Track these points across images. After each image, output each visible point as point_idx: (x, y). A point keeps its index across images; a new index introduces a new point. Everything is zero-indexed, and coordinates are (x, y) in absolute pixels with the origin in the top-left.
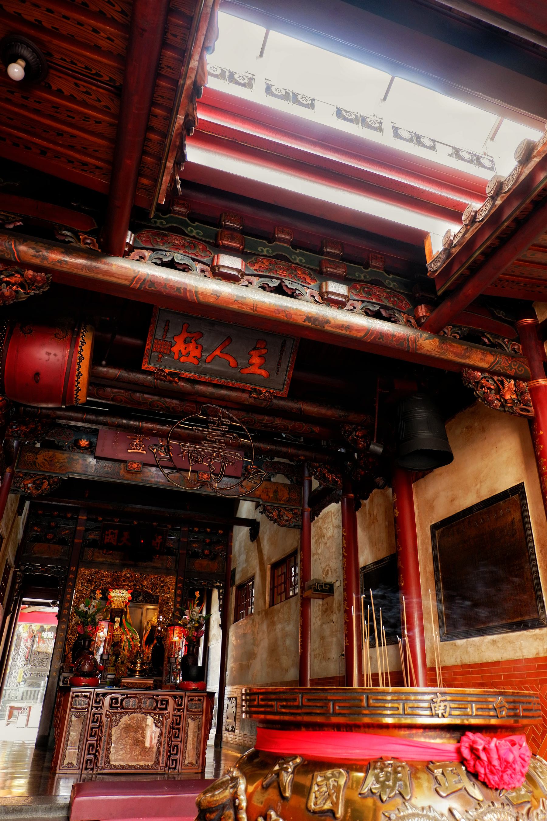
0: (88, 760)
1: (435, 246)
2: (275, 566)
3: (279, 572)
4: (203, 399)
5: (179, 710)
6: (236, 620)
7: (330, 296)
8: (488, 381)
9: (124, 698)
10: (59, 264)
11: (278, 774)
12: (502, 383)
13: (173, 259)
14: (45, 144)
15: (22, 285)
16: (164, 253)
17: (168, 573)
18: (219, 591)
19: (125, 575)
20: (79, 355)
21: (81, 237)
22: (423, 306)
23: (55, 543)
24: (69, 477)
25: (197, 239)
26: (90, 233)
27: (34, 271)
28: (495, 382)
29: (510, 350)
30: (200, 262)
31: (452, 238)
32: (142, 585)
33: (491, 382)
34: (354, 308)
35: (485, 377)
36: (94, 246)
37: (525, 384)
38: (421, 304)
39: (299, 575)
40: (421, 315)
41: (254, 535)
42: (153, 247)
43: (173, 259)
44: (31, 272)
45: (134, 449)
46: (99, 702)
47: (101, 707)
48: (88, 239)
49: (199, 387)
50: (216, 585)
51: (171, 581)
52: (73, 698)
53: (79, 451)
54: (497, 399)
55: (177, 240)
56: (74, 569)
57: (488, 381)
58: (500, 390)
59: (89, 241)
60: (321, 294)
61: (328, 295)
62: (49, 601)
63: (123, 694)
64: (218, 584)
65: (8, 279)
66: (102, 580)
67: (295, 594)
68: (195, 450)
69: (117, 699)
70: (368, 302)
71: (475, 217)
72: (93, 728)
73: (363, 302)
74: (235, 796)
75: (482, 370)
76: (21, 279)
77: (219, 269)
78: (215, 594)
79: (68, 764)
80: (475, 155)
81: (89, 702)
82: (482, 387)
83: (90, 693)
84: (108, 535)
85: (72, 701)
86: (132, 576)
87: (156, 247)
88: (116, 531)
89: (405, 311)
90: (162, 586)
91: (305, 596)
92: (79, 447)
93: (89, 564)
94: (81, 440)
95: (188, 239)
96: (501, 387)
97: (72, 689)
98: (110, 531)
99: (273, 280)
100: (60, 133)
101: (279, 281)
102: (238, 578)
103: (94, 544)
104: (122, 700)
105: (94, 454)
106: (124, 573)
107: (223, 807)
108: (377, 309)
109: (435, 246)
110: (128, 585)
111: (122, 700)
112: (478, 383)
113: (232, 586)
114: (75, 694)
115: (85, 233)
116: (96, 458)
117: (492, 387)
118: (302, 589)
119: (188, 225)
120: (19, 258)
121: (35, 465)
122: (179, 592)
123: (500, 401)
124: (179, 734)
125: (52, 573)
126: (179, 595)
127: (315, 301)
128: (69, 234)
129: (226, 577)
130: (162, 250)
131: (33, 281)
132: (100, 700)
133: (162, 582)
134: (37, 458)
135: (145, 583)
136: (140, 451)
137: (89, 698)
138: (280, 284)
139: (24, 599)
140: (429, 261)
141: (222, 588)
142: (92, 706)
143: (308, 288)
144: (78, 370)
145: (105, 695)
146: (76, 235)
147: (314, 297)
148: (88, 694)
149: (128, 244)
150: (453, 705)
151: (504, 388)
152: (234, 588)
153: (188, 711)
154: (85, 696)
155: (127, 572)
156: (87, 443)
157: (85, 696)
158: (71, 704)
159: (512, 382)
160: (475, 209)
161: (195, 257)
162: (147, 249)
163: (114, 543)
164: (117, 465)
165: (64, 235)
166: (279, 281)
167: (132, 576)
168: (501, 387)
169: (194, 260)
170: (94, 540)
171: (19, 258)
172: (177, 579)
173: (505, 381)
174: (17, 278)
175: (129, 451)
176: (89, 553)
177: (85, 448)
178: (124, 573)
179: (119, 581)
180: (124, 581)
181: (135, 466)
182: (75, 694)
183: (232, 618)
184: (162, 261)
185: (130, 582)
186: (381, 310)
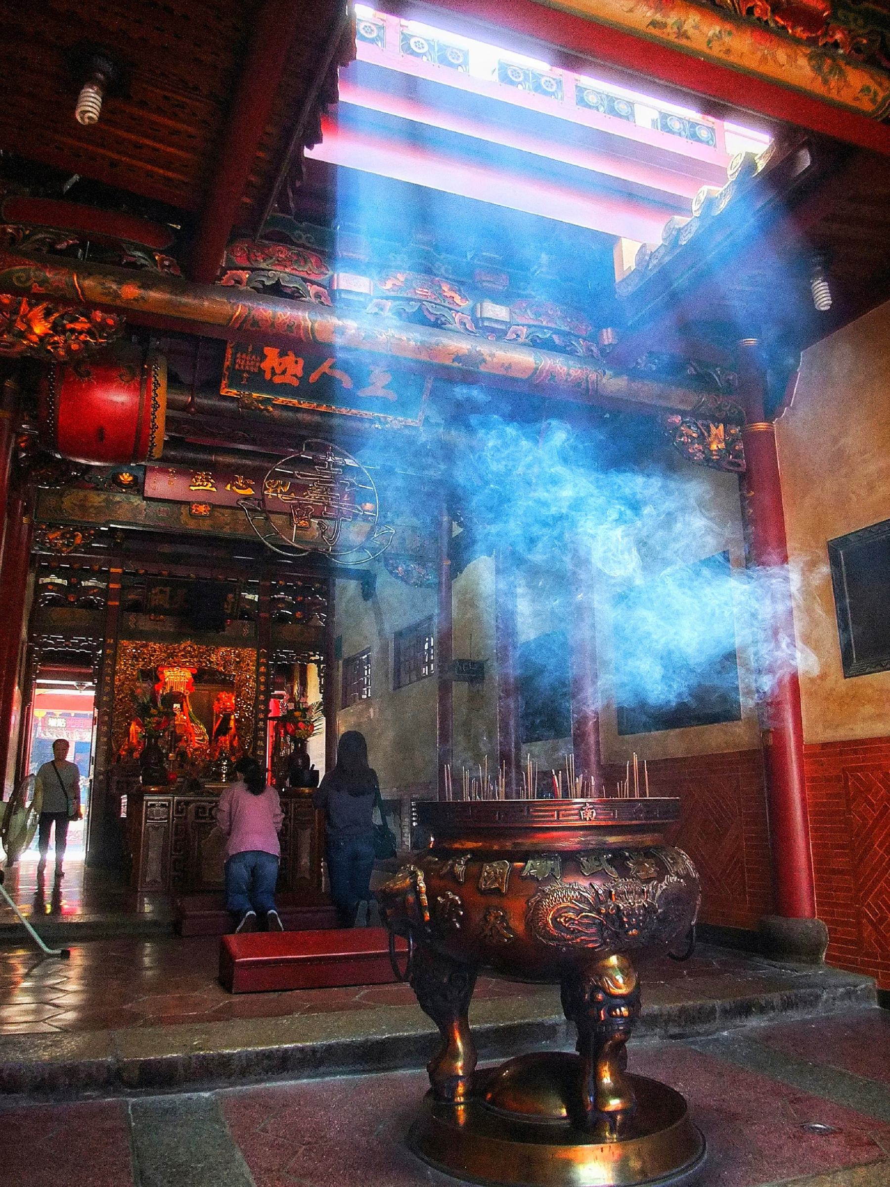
1: (628, 257)
4: (304, 433)
8: (689, 427)
11: (452, 866)
13: (278, 282)
14: (115, 156)
15: (90, 333)
17: (243, 643)
18: (319, 667)
19: (185, 648)
20: (153, 402)
22: (609, 330)
24: (110, 528)
25: (308, 248)
28: (698, 428)
31: (647, 258)
34: (518, 336)
38: (607, 328)
40: (606, 343)
42: (251, 266)
43: (278, 282)
44: (99, 314)
45: (199, 485)
46: (181, 812)
49: (300, 416)
50: (313, 658)
51: (250, 654)
53: (119, 489)
54: (700, 450)
56: (112, 641)
57: (689, 427)
59: (167, 263)
60: (475, 321)
61: (483, 322)
64: (317, 657)
65: (72, 326)
66: (153, 656)
67: (430, 675)
68: (300, 504)
69: (204, 808)
70: (535, 326)
71: (677, 239)
73: (529, 326)
74: (415, 884)
75: (683, 414)
76: (89, 325)
77: (340, 294)
78: (313, 671)
80: (689, 122)
82: (682, 436)
83: (169, 801)
86: (194, 650)
87: (255, 265)
88: (168, 589)
89: (584, 334)
90: (238, 662)
92: (121, 484)
93: (132, 635)
95: (296, 250)
96: (706, 434)
98: (158, 589)
99: (411, 303)
101: (419, 304)
104: (211, 810)
109: (628, 257)
110: (189, 661)
111: (211, 810)
115: (161, 252)
117: (694, 435)
118: (441, 669)
121: (61, 512)
122: (262, 669)
123: (703, 453)
126: (263, 674)
127: (467, 329)
130: (263, 270)
131: (103, 326)
132: (182, 809)
134: (62, 502)
135: (214, 658)
138: (420, 308)
139: (38, 681)
140: (618, 278)
141: (323, 662)
143: (458, 312)
146: (150, 254)
148: (167, 803)
151: (709, 436)
153: (295, 819)
154: (163, 806)
155: (186, 644)
156: (131, 478)
157: (163, 806)
159: (721, 427)
160: (677, 227)
161: (306, 276)
162: (243, 269)
163: (167, 606)
164: (175, 508)
165: (134, 256)
166: (419, 304)
167: (194, 650)
168: (706, 434)
172: (258, 652)
174: (82, 324)
175: (192, 488)
176: (131, 620)
177: (128, 486)
178: (183, 646)
180: (184, 656)
181: (202, 509)
183: (339, 700)
184: (264, 285)
186: (554, 336)
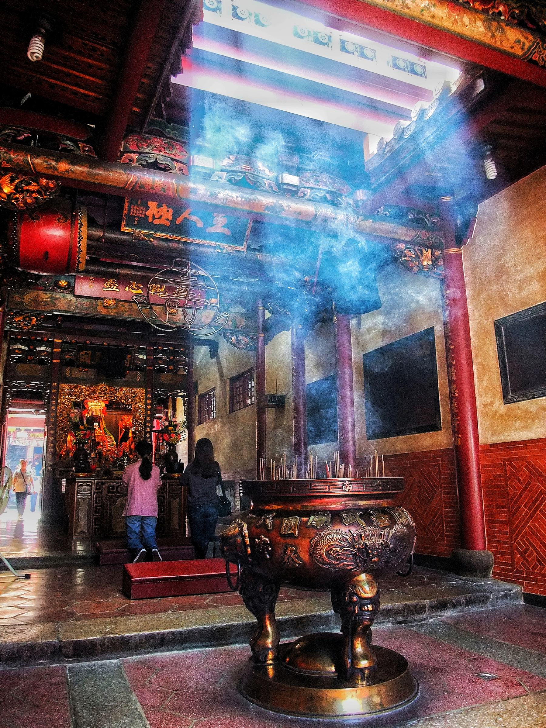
0: (95, 529)
2: (233, 380)
3: (237, 384)
5: (162, 493)
6: (200, 423)
7: (285, 187)
8: (410, 251)
9: (119, 486)
10: (67, 173)
11: (264, 520)
12: (421, 251)
13: (156, 160)
15: (38, 192)
16: (148, 155)
17: (138, 385)
21: (80, 145)
23: (35, 363)
24: (53, 314)
26: (87, 142)
27: (47, 179)
28: (416, 252)
29: (431, 223)
30: (177, 161)
31: (384, 146)
32: (116, 396)
33: (413, 252)
35: (408, 248)
36: (91, 152)
37: (439, 252)
39: (255, 387)
41: (214, 353)
43: (156, 160)
44: (45, 180)
45: (109, 288)
47: (102, 492)
48: (86, 147)
50: (180, 394)
52: (78, 486)
53: (59, 290)
55: (158, 142)
58: (419, 258)
59: (87, 149)
62: (33, 410)
63: (117, 483)
64: (183, 394)
66: (81, 393)
67: (252, 404)
69: (113, 486)
72: (96, 507)
74: (241, 531)
76: (38, 187)
78: (180, 402)
79: (81, 531)
80: (410, 62)
81: (91, 489)
82: (405, 256)
83: (92, 482)
84: (82, 355)
85: (78, 489)
86: (107, 389)
90: (134, 397)
91: (261, 406)
92: (59, 287)
93: (68, 381)
94: (60, 281)
95: (167, 141)
97: (77, 481)
100: (69, 75)
102: (201, 389)
103: (71, 363)
105: (74, 292)
106: (100, 387)
107: (235, 536)
108: (323, 194)
112: (402, 252)
113: (195, 395)
114: (79, 484)
116: (75, 296)
117: (413, 256)
119: (166, 127)
120: (35, 170)
124: (164, 509)
125: (37, 388)
128: (70, 143)
129: (189, 385)
131: (46, 188)
133: (134, 393)
134: (23, 299)
136: (114, 289)
137: (91, 486)
142: (94, 492)
144: (79, 248)
145: (103, 484)
146: (75, 142)
147: (272, 188)
149: (120, 151)
150: (354, 486)
152: (197, 397)
154: (88, 485)
156: (66, 284)
157: (88, 485)
158: (77, 491)
159: (430, 250)
160: (402, 127)
168: (420, 255)
169: (173, 160)
170: (70, 359)
171: (35, 170)
173: (424, 250)
174: (34, 187)
176: (68, 372)
177: (64, 288)
179: (96, 393)
181: (110, 302)
182: (79, 484)
185: (105, 394)
